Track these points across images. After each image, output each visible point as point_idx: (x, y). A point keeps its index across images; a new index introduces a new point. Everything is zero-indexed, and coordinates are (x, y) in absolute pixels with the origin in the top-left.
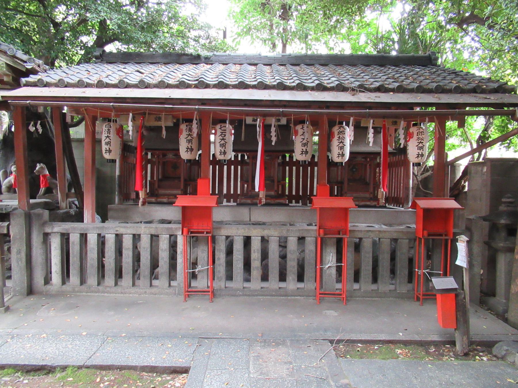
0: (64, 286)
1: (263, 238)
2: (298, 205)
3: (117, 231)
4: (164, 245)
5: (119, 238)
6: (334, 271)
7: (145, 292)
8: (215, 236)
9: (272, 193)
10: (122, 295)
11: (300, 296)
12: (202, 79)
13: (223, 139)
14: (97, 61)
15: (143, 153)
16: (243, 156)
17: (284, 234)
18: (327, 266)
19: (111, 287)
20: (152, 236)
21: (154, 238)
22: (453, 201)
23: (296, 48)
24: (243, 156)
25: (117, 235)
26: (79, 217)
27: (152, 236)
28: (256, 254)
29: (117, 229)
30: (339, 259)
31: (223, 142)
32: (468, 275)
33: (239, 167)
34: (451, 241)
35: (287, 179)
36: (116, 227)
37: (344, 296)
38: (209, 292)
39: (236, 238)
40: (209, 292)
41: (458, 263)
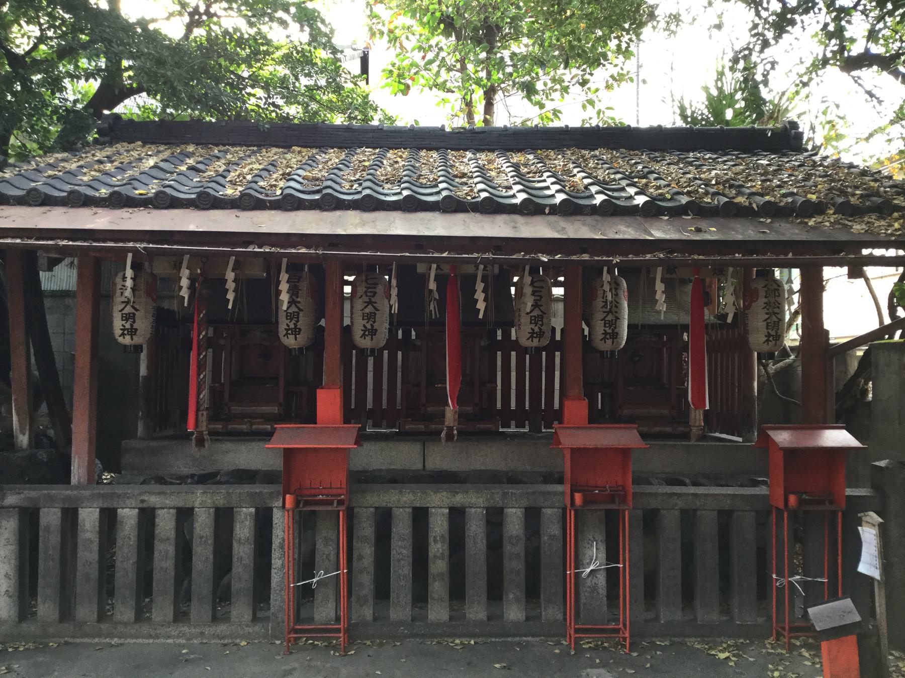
0: (24, 625)
1: (452, 510)
2: (522, 430)
3: (143, 501)
4: (244, 529)
5: (147, 516)
6: (601, 580)
7: (202, 634)
8: (353, 508)
9: (469, 409)
10: (151, 641)
11: (533, 636)
12: (329, 191)
13: (370, 303)
14: (102, 139)
15: (204, 333)
16: (407, 334)
17: (498, 500)
18: (588, 570)
19: (125, 624)
20: (218, 510)
21: (224, 518)
22: (844, 432)
23: (514, 110)
24: (407, 334)
25: (142, 511)
26: (60, 473)
27: (218, 510)
28: (439, 545)
29: (142, 498)
30: (612, 555)
31: (369, 309)
32: (883, 595)
33: (400, 354)
34: (843, 513)
35: (499, 374)
36: (141, 494)
37: (627, 635)
38: (338, 631)
39: (396, 512)
40: (338, 631)
41: (862, 568)
